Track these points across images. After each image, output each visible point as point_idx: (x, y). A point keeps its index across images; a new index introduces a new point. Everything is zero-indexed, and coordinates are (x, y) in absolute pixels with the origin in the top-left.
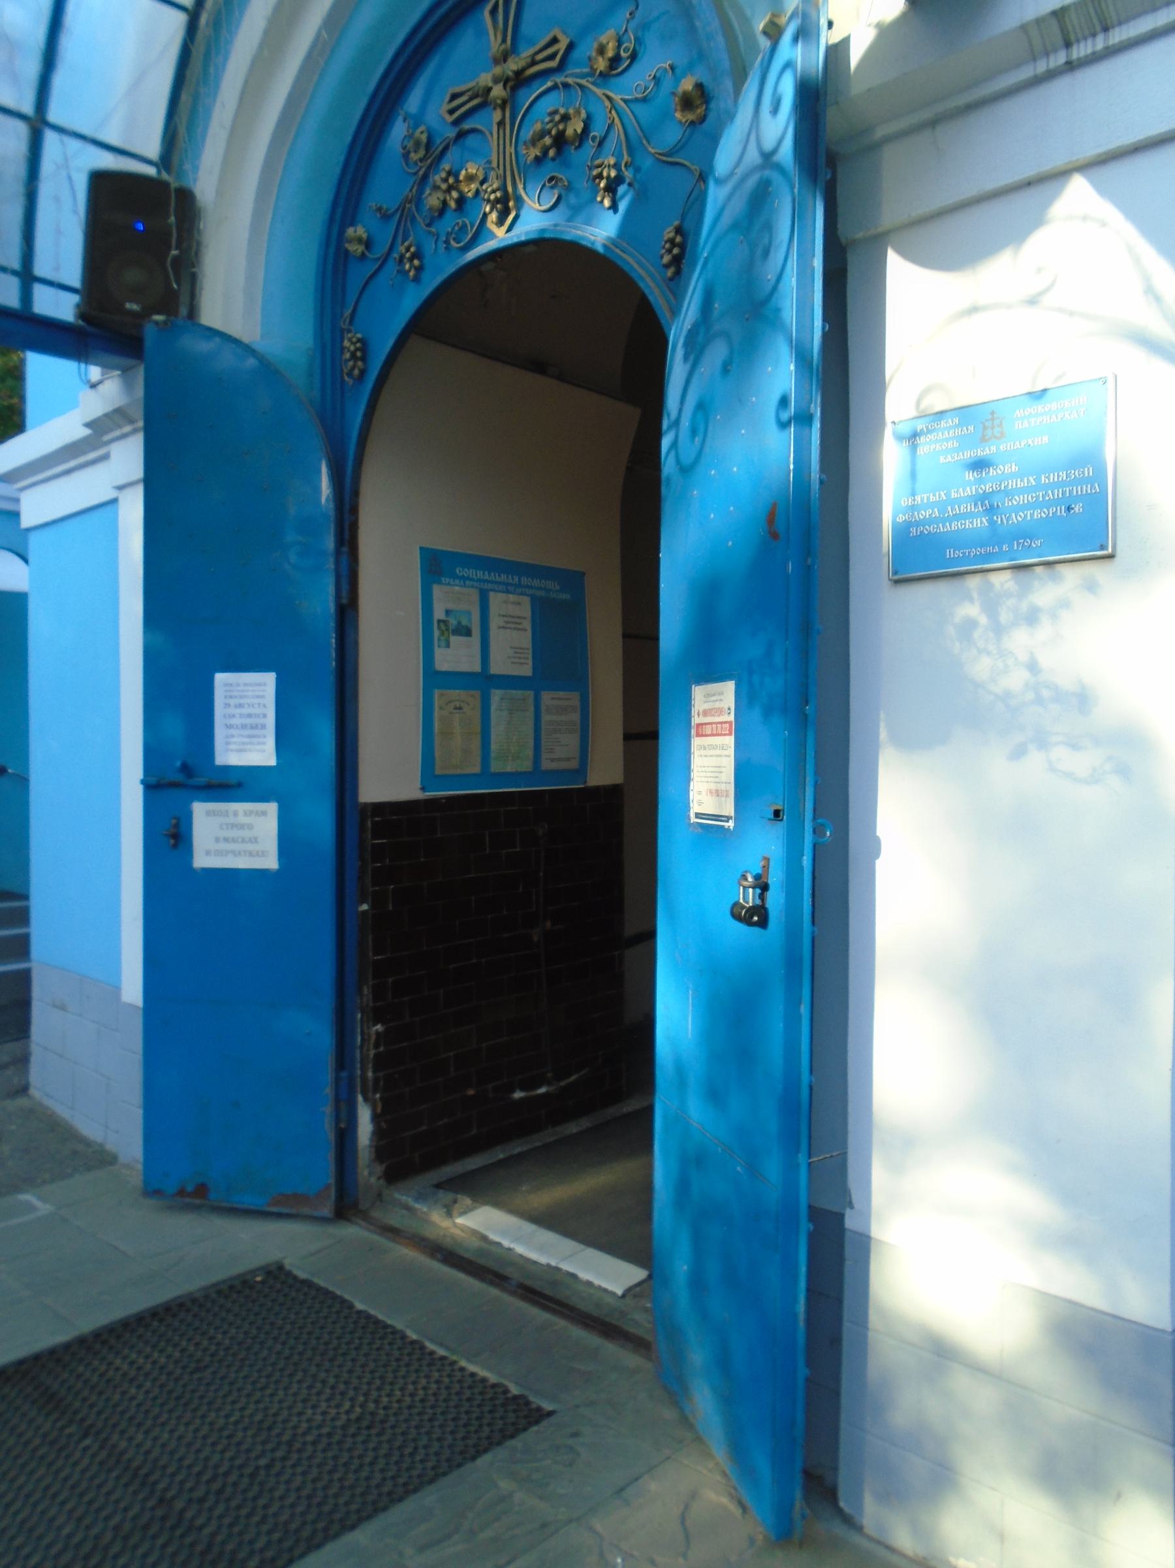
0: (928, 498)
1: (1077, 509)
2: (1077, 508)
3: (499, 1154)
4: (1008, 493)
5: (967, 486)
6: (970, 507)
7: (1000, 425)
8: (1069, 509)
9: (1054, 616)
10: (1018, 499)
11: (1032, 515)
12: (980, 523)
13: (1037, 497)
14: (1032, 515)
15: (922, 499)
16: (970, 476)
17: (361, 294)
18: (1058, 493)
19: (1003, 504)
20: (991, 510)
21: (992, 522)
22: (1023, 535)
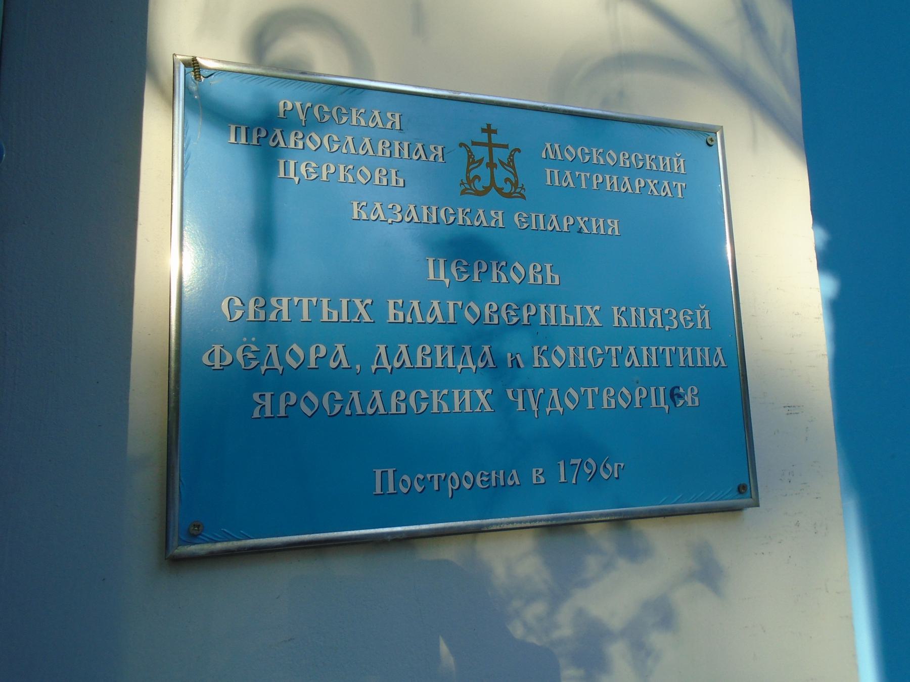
0: (315, 310)
1: (688, 398)
2: (689, 398)
3: (173, 364)
4: (545, 336)
5: (437, 294)
6: (444, 357)
7: (510, 164)
8: (674, 395)
9: (635, 637)
10: (562, 355)
11: (597, 398)
12: (471, 398)
13: (606, 355)
14: (597, 398)
15: (295, 309)
16: (437, 273)
17: (181, 255)
18: (647, 356)
19: (529, 361)
20: (500, 371)
21: (501, 403)
22: (573, 443)
